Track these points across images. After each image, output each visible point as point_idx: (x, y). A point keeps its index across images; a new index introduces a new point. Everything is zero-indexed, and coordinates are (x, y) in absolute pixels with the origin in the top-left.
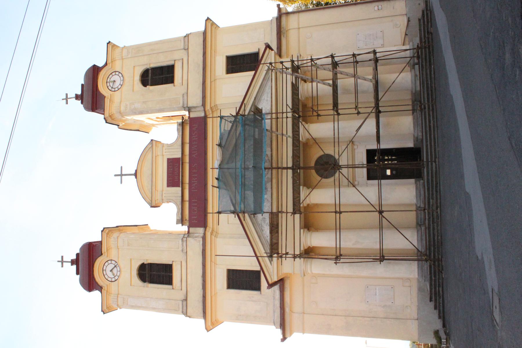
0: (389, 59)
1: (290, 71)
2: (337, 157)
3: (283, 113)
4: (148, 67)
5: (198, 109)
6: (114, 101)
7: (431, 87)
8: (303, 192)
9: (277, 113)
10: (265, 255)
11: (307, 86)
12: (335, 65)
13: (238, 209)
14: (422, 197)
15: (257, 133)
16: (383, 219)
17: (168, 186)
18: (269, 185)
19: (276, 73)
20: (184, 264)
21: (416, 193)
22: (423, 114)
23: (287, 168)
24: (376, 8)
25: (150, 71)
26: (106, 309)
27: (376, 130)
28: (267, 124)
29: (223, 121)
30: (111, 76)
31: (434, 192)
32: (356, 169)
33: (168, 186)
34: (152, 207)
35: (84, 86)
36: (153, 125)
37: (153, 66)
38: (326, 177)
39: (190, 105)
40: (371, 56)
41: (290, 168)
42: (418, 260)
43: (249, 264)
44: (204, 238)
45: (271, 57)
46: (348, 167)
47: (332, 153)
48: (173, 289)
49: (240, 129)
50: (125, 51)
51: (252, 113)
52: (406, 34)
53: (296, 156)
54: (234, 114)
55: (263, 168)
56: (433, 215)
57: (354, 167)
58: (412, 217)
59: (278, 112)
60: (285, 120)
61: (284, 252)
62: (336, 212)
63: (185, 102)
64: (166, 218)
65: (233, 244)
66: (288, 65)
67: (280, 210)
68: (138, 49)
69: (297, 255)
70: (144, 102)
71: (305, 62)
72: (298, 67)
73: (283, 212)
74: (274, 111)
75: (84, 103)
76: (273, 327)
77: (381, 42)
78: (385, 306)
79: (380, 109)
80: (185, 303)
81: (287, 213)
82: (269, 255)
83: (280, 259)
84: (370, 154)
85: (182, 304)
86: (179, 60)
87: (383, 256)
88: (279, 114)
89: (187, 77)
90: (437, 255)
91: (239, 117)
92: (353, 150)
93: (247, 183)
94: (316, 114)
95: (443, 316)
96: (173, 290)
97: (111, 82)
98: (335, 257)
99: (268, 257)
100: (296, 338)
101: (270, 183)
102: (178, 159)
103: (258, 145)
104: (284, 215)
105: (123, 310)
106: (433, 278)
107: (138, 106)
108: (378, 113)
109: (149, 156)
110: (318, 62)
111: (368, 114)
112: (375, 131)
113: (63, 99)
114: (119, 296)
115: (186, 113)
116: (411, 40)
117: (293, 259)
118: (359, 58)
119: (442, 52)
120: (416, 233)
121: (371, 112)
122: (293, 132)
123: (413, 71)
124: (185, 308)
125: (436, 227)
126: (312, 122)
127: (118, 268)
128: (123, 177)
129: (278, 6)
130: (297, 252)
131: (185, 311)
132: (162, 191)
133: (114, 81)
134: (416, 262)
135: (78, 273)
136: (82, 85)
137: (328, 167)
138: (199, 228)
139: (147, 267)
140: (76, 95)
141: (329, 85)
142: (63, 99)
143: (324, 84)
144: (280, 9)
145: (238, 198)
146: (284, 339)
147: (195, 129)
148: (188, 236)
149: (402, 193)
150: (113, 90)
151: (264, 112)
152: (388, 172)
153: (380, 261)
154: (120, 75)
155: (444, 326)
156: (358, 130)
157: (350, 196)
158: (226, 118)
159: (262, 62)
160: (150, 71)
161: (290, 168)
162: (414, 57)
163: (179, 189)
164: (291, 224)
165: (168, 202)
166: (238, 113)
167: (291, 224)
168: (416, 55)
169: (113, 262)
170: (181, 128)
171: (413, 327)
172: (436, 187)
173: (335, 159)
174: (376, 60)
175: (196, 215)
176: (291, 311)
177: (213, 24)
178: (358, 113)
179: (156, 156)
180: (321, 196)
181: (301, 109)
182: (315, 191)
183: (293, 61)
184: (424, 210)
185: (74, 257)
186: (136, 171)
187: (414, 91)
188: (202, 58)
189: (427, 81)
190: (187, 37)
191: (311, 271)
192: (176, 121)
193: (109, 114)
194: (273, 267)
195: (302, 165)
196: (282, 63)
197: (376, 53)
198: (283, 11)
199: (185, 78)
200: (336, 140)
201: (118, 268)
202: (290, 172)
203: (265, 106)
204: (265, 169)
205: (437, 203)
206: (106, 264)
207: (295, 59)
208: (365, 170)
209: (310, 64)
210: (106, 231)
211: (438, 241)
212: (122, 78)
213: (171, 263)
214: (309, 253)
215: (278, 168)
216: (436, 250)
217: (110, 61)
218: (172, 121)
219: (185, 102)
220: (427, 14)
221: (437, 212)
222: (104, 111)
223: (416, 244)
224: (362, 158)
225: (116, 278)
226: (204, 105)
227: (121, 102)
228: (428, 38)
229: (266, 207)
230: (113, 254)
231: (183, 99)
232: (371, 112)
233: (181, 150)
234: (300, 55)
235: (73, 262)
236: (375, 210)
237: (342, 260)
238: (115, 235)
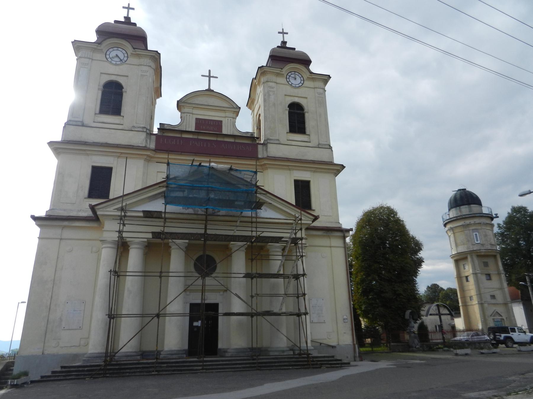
0: (300, 327)
1: (294, 236)
2: (213, 275)
3: (256, 228)
4: (305, 111)
5: (265, 152)
7: (272, 366)
9: (257, 222)
10: (124, 204)
11: (278, 251)
12: (297, 277)
13: (170, 182)
14: (170, 356)
15: (239, 203)
16: (151, 318)
17: (197, 119)
18: (190, 211)
19: (292, 224)
20: (120, 127)
21: (175, 350)
22: (248, 358)
23: (206, 229)
24: (345, 317)
25: (302, 112)
26: (78, 46)
27: (235, 312)
28: (248, 213)
29: (253, 174)
31: (173, 368)
32: (201, 293)
33: (197, 119)
34: (178, 102)
35: (294, 51)
36: (253, 111)
37: (306, 115)
38: (195, 265)
39: (269, 146)
40: (303, 310)
41: (206, 231)
42: (107, 352)
43: (116, 189)
45: (306, 220)
46: (204, 285)
47: (218, 270)
48: (96, 114)
49: (244, 188)
50: (321, 91)
51: (257, 200)
52: (321, 344)
53: (216, 237)
54: (258, 184)
55: (207, 207)
56: (151, 367)
57: (203, 291)
58: (150, 346)
59: (258, 224)
60: (250, 229)
61: (125, 222)
62: (161, 272)
65: (130, 177)
66: (299, 235)
67: (167, 220)
68: (322, 102)
69: (122, 235)
70: (274, 105)
71: (301, 250)
72: (296, 244)
73: (165, 223)
74: (258, 220)
75: (278, 49)
76: (48, 209)
77: (315, 320)
78: (61, 319)
79: (255, 318)
80: (80, 124)
81: (164, 227)
82: (124, 208)
83: (119, 218)
84: (214, 307)
85: (79, 121)
87: (113, 318)
88: (255, 224)
89: (291, 146)
90: (111, 372)
91: (255, 188)
92: (218, 291)
93: (195, 191)
94: (253, 258)
95: (44, 380)
96: (94, 113)
98: (117, 270)
99: (122, 207)
100: (35, 230)
101: (193, 213)
103: (229, 204)
104: (162, 224)
105: (75, 62)
106: (86, 369)
107: (272, 97)
108: (251, 315)
109: (225, 105)
110: (300, 262)
111: (250, 304)
113: (283, 29)
114: (91, 60)
115: (262, 142)
116: (315, 348)
117: (118, 230)
118: (301, 299)
119: (304, 376)
120: (134, 351)
121: (252, 308)
122: (239, 236)
123: (288, 349)
124: (74, 123)
125: (138, 370)
126: (247, 254)
127: (119, 63)
129: (351, 230)
130: (125, 235)
131: (71, 123)
132: (193, 114)
133: (295, 79)
134: (105, 351)
135: (116, 22)
136: (294, 49)
137: (205, 264)
139: (292, 111)
140: (286, 42)
141: (279, 270)
142: (283, 29)
143: (280, 266)
144: (348, 231)
145: (182, 183)
146: (34, 218)
147: (247, 147)
148: (147, 134)
149: (174, 337)
151: (258, 211)
153: (109, 315)
154: (300, 85)
155: (32, 382)
156: (236, 295)
157: (174, 286)
158: (255, 177)
159: (302, 212)
160: (302, 112)
161: (206, 231)
162: (300, 350)
163: (193, 129)
165: (181, 117)
166: (258, 187)
168: (302, 352)
169: (125, 59)
170: (249, 135)
171: (35, 350)
172: (178, 370)
173: (212, 274)
174: (299, 315)
175: (168, 141)
177: (339, 172)
178: (252, 297)
179: (225, 110)
180: (177, 261)
181: (259, 244)
182: (184, 253)
183: (301, 239)
184: (157, 359)
185: (132, 21)
186: (213, 91)
187: (269, 349)
189: (278, 362)
190: (329, 147)
191: (105, 247)
192: (255, 131)
194: (111, 211)
195: (208, 242)
196: (301, 229)
197: (305, 315)
198: (346, 234)
199: (294, 143)
200: (229, 275)
201: (119, 63)
202: (202, 231)
203: (265, 213)
204: (207, 209)
205: (162, 371)
207: (304, 241)
208: (199, 301)
209: (298, 254)
210: (156, 56)
211: (124, 373)
213: (122, 114)
214: (122, 247)
215: (206, 220)
216: (115, 371)
218: (256, 128)
219: (271, 142)
220: (338, 364)
221: (153, 371)
222: (269, 67)
223: (123, 350)
224: (211, 299)
225: (109, 60)
226: (269, 158)
227: (277, 83)
228: (317, 364)
229: (171, 208)
230: (133, 60)
231: (274, 140)
232: (252, 308)
234: (306, 246)
235: (127, 19)
236: (161, 309)
237: (113, 277)
238: (153, 65)
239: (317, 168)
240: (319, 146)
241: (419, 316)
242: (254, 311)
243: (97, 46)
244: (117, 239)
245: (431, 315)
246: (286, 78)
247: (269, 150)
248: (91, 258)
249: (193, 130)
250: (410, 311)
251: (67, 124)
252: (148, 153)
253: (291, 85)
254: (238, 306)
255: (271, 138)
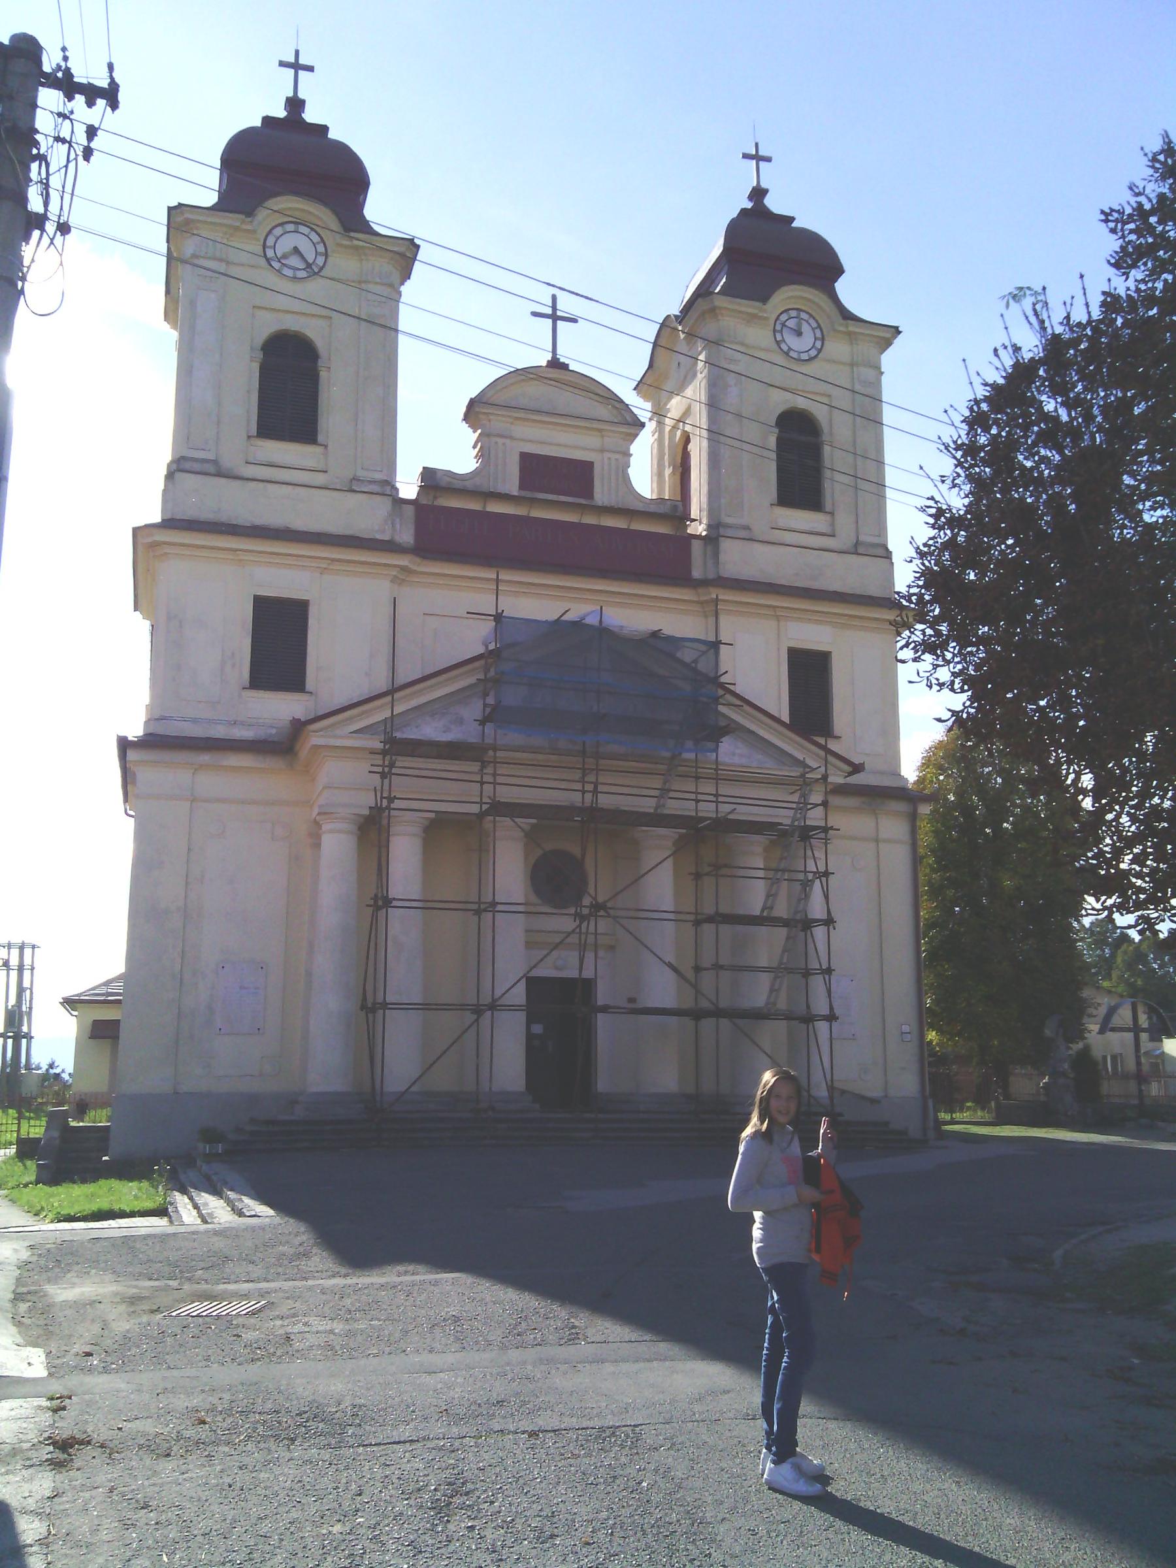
3: (716, 795)
6: (749, 328)
8: (669, 834)
17: (525, 457)
20: (320, 479)
24: (906, 1028)
30: (814, 325)
33: (525, 457)
39: (726, 545)
44: (390, 547)
48: (249, 437)
63: (730, 533)
64: (433, 438)
80: (211, 468)
86: (833, 525)
89: (784, 543)
97: (799, 325)
102: (589, 494)
109: (603, 412)
112: (651, 1004)
124: (197, 467)
127: (302, 274)
128: (550, 321)
131: (187, 465)
138: (412, 531)
140: (766, 191)
147: (654, 549)
150: (778, 327)
152: (537, 1029)
154: (813, 353)
164: (457, 792)
166: (722, 686)
167: (457, 792)
169: (320, 261)
175: (448, 525)
176: (201, 767)
179: (600, 430)
180: (510, 871)
186: (565, 367)
188: (832, 588)
191: (331, 831)
193: (720, 308)
194: (342, 737)
199: (789, 537)
201: (302, 274)
203: (730, 752)
206: (316, 238)
212: (805, 356)
213: (320, 438)
214: (372, 830)
217: (851, 329)
219: (730, 533)
233: (613, 503)
239: (850, 616)
240: (856, 549)
241: (1079, 1033)
242: (705, 1004)
243: (243, 222)
244: (366, 812)
245: (1113, 1030)
246: (775, 331)
247: (722, 557)
248: (290, 855)
249: (515, 491)
250: (50, 1289)
251: (178, 468)
252: (404, 561)
253: (787, 354)
254: (662, 989)
255: (729, 520)
